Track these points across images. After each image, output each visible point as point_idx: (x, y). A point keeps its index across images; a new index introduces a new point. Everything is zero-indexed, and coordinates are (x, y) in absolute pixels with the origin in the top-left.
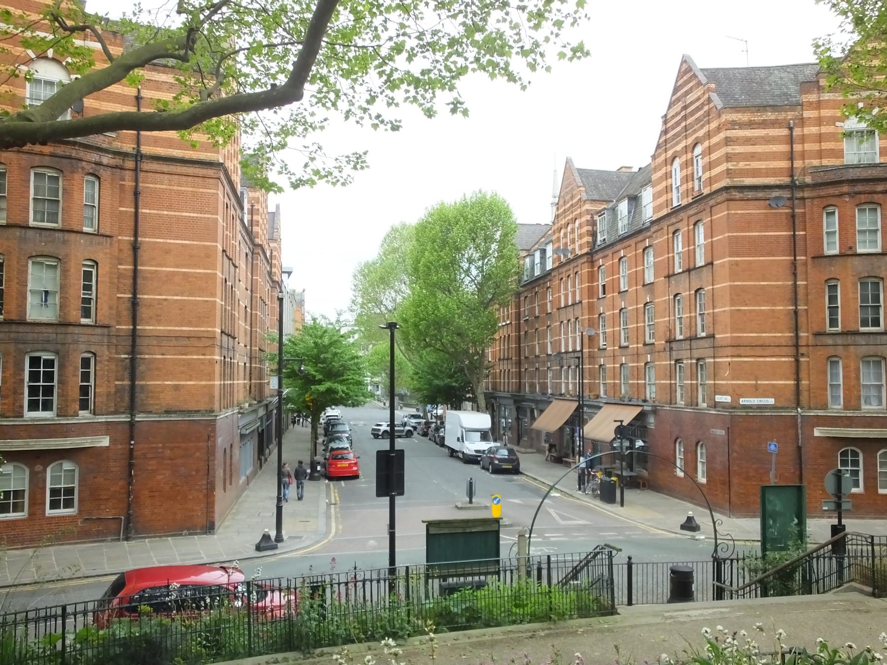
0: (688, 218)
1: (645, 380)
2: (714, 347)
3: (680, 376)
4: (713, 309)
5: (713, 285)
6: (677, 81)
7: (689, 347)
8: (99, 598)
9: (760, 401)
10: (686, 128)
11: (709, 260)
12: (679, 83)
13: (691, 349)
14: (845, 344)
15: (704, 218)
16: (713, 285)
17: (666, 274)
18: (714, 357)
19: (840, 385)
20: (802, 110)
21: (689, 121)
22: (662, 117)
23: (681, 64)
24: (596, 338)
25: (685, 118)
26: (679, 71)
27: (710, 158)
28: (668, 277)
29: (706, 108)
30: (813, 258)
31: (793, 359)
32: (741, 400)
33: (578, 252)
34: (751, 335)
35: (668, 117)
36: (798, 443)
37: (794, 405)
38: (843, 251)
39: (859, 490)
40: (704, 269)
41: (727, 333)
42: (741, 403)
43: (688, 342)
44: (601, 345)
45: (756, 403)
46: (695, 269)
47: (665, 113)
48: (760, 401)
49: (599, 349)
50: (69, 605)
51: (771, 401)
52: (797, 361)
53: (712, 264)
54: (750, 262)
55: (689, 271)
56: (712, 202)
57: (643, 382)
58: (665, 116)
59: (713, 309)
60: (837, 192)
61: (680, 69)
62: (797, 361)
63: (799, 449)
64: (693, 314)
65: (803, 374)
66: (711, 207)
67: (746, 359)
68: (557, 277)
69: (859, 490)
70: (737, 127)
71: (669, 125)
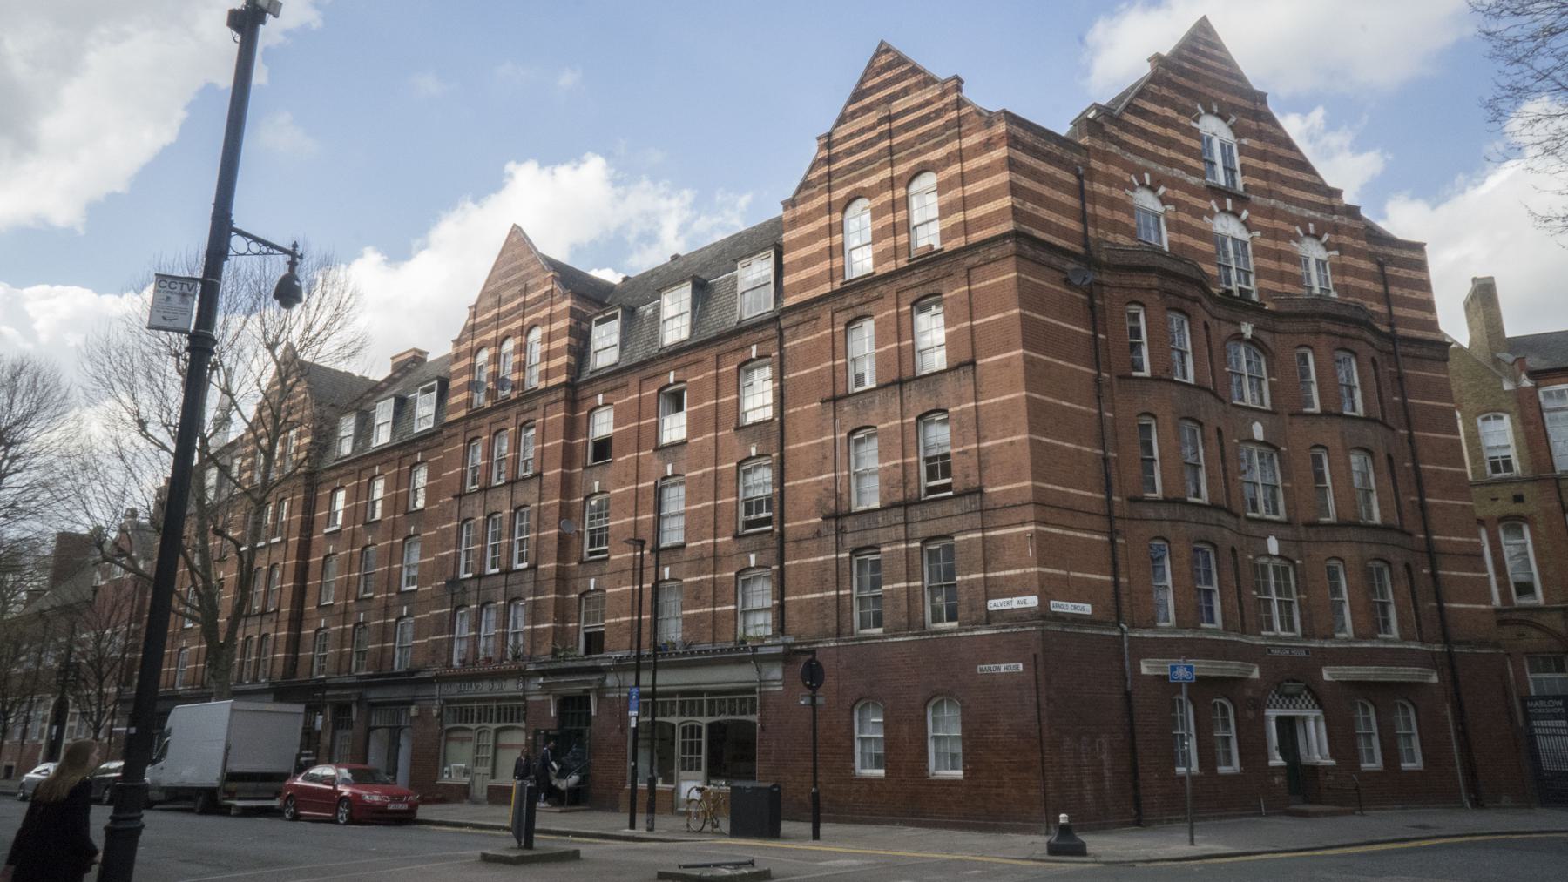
0: (897, 293)
1: (736, 604)
2: (981, 511)
3: (859, 580)
4: (978, 443)
5: (976, 400)
6: (862, 82)
7: (901, 519)
8: (1104, 103)
9: (1075, 608)
10: (891, 150)
11: (966, 357)
12: (869, 84)
13: (906, 524)
14: (1173, 517)
15: (944, 289)
16: (976, 400)
17: (828, 393)
18: (983, 529)
19: (1166, 587)
20: (1088, 156)
21: (897, 140)
22: (470, 308)
23: (877, 55)
24: (575, 541)
25: (890, 134)
26: (870, 66)
27: (963, 191)
28: (835, 399)
29: (953, 115)
30: (1119, 377)
31: (1106, 539)
32: (1052, 602)
33: (535, 382)
34: (1057, 488)
35: (836, 137)
36: (1125, 687)
37: (1114, 619)
38: (1159, 373)
39: (1235, 767)
40: (948, 377)
41: (1023, 480)
42: (1053, 609)
43: (902, 510)
44: (585, 554)
45: (1070, 611)
46: (914, 379)
47: (828, 130)
48: (1075, 608)
49: (581, 562)
50: (226, 761)
51: (1086, 609)
52: (1112, 542)
53: (973, 363)
54: (1048, 365)
55: (900, 383)
56: (970, 261)
57: (733, 607)
58: (829, 135)
59: (978, 443)
60: (1145, 284)
61: (872, 61)
62: (1112, 542)
63: (1128, 696)
64: (913, 459)
65: (1122, 568)
66: (969, 270)
67: (1053, 530)
68: (461, 437)
69: (1235, 767)
70: (1019, 147)
71: (479, 320)
